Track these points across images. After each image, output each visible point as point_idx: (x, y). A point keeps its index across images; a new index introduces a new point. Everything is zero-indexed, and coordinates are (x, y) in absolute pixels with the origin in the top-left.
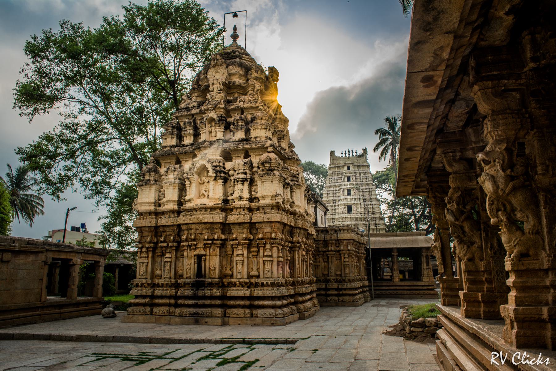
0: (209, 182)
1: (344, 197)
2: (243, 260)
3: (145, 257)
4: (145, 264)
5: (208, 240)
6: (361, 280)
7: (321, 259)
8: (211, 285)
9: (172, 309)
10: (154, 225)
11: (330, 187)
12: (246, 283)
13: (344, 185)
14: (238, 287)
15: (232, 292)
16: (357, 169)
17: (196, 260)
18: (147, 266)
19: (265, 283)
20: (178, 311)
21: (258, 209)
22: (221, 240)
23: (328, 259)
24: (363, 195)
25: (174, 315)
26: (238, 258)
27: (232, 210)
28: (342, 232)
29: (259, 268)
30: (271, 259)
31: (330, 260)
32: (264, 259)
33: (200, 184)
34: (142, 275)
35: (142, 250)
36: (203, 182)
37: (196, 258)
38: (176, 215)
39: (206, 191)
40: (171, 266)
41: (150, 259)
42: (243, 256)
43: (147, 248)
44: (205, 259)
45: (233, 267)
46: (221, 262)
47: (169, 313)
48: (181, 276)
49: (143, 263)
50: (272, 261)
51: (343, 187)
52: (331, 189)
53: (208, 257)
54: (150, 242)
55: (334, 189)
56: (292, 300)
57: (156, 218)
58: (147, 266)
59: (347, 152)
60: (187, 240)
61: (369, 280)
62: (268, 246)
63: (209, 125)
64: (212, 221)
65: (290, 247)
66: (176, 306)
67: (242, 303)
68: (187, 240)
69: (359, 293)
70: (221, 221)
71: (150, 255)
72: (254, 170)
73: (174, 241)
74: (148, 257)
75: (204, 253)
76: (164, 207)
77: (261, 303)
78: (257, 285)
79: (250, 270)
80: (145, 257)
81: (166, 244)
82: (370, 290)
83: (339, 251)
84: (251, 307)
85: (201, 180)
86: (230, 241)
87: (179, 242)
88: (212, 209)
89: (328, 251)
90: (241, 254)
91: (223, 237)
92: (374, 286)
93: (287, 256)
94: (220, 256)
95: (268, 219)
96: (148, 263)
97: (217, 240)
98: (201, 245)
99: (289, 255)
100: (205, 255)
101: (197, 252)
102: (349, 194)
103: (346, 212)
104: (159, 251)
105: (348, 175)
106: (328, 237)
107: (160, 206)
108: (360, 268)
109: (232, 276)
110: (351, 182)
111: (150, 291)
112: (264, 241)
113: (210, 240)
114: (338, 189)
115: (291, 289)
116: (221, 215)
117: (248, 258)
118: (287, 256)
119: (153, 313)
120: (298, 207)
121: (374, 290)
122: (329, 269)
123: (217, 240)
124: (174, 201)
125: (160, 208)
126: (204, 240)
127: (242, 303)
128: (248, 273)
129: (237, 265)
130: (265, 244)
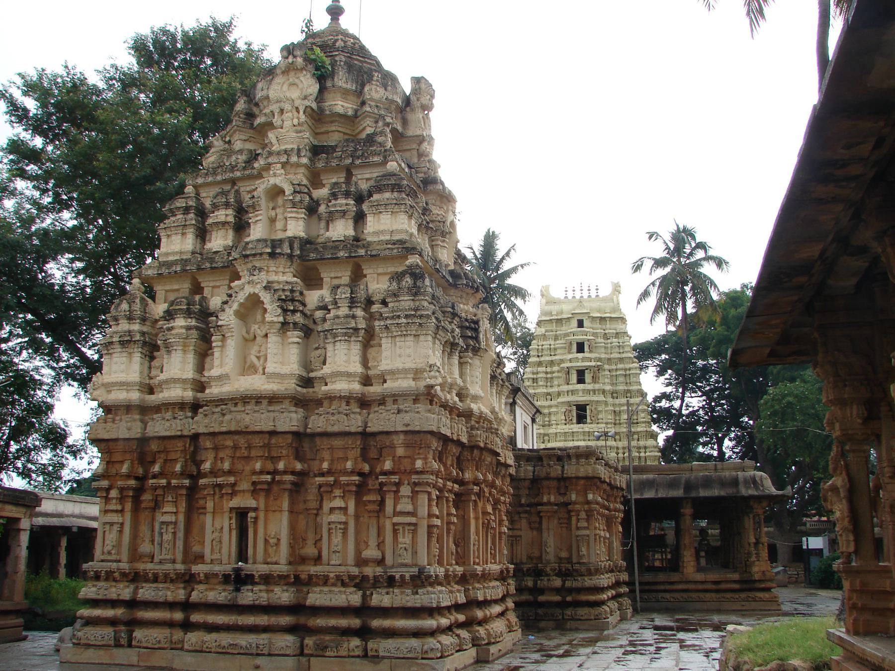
0: (266, 335)
1: (570, 387)
2: (346, 523)
3: (116, 511)
4: (116, 528)
5: (261, 472)
6: (612, 571)
7: (524, 523)
8: (267, 579)
9: (178, 634)
10: (139, 436)
11: (540, 364)
12: (352, 577)
13: (570, 361)
14: (334, 585)
15: (317, 597)
16: (598, 326)
17: (233, 521)
18: (121, 532)
19: (397, 577)
20: (193, 638)
21: (382, 402)
22: (293, 473)
23: (540, 523)
24: (612, 384)
25: (182, 649)
26: (333, 518)
27: (319, 403)
28: (574, 460)
29: (383, 542)
30: (413, 520)
31: (544, 526)
32: (396, 520)
33: (246, 340)
34: (109, 553)
35: (108, 493)
36: (252, 336)
37: (234, 515)
38: (190, 414)
39: (258, 358)
40: (174, 533)
41: (128, 516)
42: (346, 514)
43: (122, 490)
44: (256, 518)
45: (321, 539)
46: (293, 527)
47: (171, 642)
48: (199, 558)
49: (112, 524)
50: (415, 525)
51: (569, 364)
52: (540, 369)
53: (262, 515)
54: (128, 476)
55: (549, 369)
56: (461, 618)
57: (142, 421)
58: (121, 532)
59: (578, 289)
60: (213, 473)
61: (630, 569)
62: (405, 490)
63: (271, 205)
64: (271, 428)
65: (456, 494)
66: (187, 626)
67: (343, 622)
68: (213, 473)
69: (609, 599)
70: (294, 429)
71: (128, 506)
72: (375, 308)
73: (183, 474)
74: (122, 511)
75: (252, 503)
76: (161, 395)
77: (387, 623)
78: (376, 583)
79: (363, 546)
80: (116, 511)
81: (163, 482)
82: (632, 591)
83: (566, 504)
84: (364, 633)
85: (248, 332)
86: (315, 476)
87: (195, 478)
88: (273, 399)
89: (542, 504)
90: (340, 508)
91: (299, 466)
92: (640, 583)
93: (449, 514)
94: (291, 512)
95: (407, 425)
96: (122, 524)
97: (285, 472)
98: (245, 485)
99: (454, 511)
100: (255, 509)
101: (236, 502)
102: (581, 381)
103: (575, 421)
104: (147, 497)
105: (580, 338)
106: (542, 472)
107: (151, 391)
108: (611, 543)
109: (318, 560)
110: (586, 355)
111: (127, 590)
112: (395, 478)
113: (268, 473)
114: (556, 368)
115: (459, 591)
116: (294, 415)
117: (357, 517)
118: (449, 514)
119: (134, 643)
120: (475, 398)
121: (641, 591)
122: (541, 545)
123: (285, 472)
124: (184, 381)
125: (153, 397)
126: (254, 473)
127: (343, 622)
128: (358, 552)
129: (330, 534)
130: (398, 485)
